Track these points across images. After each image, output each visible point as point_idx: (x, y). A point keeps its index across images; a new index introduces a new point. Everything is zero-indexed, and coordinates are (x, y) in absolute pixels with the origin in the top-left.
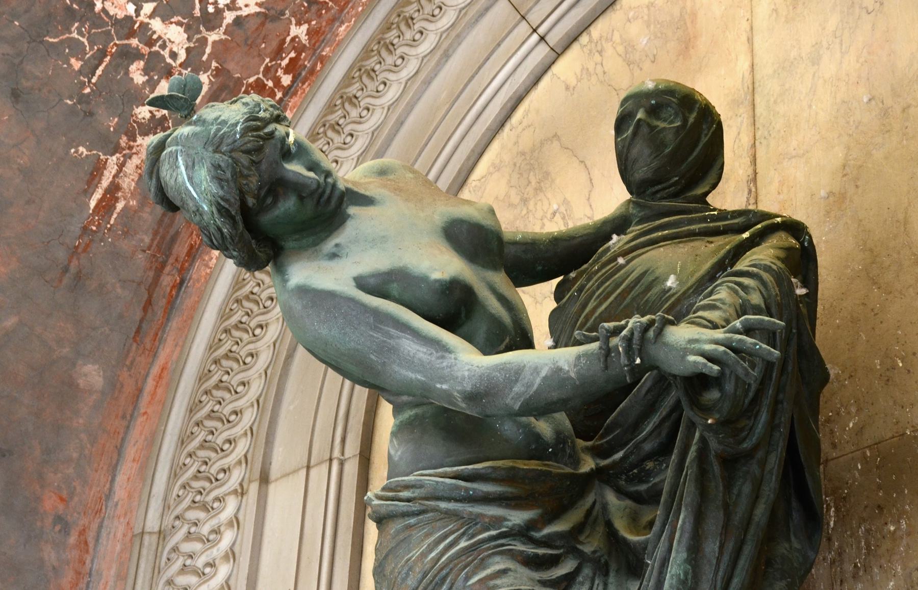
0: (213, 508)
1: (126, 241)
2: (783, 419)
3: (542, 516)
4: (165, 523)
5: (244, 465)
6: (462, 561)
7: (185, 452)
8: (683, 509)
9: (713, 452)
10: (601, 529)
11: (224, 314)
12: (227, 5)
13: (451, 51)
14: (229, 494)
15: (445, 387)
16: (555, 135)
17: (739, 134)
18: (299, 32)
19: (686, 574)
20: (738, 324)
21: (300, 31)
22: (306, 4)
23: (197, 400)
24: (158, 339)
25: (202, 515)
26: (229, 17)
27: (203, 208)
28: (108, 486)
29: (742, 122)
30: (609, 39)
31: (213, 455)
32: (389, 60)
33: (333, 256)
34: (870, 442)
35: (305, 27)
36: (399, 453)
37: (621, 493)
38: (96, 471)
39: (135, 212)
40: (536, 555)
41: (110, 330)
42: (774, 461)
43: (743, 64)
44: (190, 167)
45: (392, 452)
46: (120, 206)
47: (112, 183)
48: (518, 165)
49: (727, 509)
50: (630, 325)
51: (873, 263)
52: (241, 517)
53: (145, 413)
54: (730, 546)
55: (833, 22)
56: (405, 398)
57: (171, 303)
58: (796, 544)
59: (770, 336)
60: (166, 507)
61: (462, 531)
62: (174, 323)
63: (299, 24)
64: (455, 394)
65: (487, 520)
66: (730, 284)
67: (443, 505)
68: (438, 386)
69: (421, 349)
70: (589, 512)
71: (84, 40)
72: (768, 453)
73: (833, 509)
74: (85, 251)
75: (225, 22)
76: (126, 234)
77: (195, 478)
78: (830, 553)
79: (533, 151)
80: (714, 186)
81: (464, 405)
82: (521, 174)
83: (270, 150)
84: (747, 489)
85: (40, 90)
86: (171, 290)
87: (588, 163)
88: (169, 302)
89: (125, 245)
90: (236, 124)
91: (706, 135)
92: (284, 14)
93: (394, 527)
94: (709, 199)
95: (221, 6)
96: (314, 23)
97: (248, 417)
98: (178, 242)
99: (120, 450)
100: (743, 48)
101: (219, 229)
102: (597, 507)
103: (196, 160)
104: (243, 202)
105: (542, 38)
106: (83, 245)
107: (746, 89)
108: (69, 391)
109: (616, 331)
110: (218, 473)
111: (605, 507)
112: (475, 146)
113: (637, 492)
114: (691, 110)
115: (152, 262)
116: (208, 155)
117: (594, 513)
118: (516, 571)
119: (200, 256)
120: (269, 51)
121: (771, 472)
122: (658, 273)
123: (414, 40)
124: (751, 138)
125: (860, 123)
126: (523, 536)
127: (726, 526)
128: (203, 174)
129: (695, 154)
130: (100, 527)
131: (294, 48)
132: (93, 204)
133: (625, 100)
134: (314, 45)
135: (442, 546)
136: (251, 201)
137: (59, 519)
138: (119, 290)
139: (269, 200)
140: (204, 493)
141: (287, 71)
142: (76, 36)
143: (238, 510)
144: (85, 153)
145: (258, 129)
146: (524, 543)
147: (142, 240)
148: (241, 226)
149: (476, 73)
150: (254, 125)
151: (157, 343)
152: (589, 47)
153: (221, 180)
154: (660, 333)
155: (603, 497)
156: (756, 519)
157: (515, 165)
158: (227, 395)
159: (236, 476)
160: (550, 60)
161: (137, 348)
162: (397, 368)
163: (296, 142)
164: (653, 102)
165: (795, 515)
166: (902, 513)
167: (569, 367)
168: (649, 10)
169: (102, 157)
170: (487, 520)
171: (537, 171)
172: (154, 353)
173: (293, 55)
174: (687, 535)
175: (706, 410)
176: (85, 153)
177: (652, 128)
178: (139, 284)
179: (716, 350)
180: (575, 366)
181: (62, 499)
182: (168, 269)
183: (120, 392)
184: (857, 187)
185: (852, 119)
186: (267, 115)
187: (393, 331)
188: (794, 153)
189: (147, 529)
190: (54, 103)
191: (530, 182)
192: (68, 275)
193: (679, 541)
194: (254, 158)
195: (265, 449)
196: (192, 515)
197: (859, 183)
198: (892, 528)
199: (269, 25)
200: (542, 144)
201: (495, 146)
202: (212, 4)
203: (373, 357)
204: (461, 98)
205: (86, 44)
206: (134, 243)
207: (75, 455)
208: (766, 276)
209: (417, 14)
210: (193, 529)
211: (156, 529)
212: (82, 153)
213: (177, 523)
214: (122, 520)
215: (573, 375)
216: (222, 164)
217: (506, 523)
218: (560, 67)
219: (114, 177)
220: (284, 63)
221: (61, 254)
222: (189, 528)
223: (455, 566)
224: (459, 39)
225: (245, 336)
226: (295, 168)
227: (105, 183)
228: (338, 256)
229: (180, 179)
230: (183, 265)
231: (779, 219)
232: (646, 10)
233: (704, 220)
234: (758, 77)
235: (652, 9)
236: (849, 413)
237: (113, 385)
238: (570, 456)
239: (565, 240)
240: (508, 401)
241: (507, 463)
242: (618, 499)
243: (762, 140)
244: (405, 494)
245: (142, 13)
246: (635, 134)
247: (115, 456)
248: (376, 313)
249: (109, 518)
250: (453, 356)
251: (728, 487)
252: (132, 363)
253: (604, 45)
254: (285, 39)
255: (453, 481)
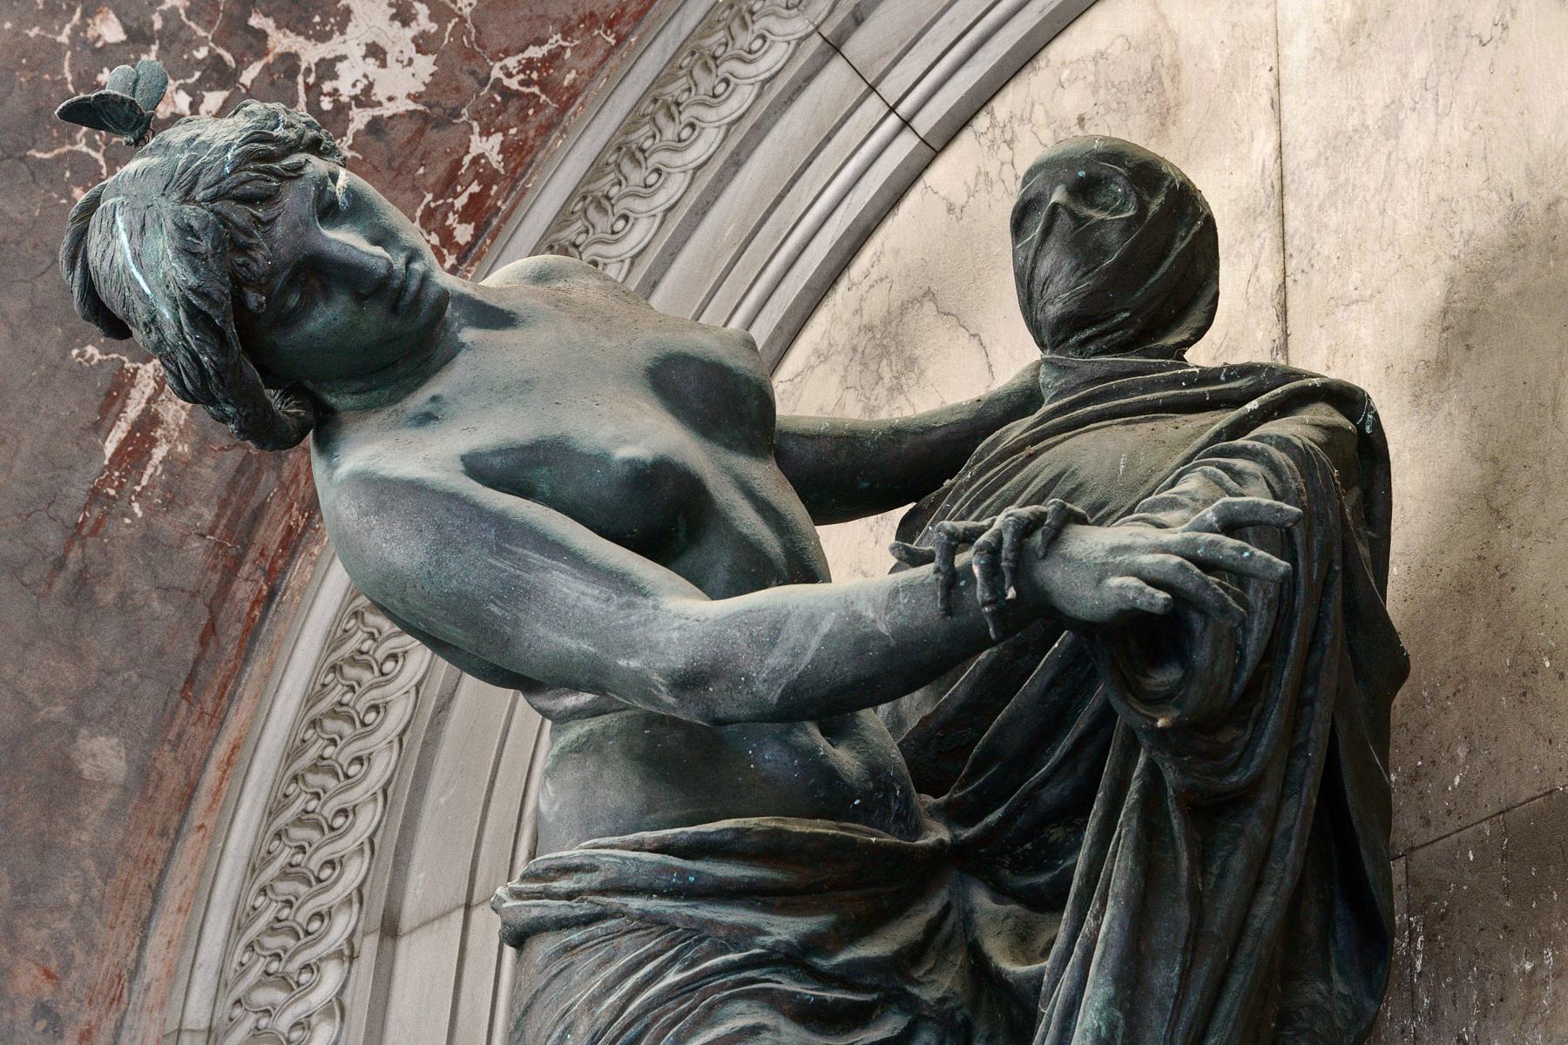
0: (298, 984)
1: (169, 517)
2: (1312, 734)
3: (836, 927)
4: (218, 1015)
5: (356, 907)
6: (669, 1011)
7: (256, 886)
8: (1110, 903)
9: (1171, 792)
10: (958, 959)
11: (334, 640)
12: (355, 98)
13: (742, 156)
14: (328, 957)
15: (634, 664)
16: (928, 292)
17: (1256, 267)
18: (487, 147)
19: (1112, 1027)
20: (1209, 514)
21: (488, 146)
22: (499, 99)
23: (280, 795)
24: (227, 692)
25: (280, 996)
26: (359, 119)
27: (162, 316)
28: (133, 954)
29: (1262, 247)
30: (1026, 119)
31: (303, 889)
32: (636, 176)
33: (426, 419)
34: (1491, 810)
35: (497, 139)
36: (556, 808)
37: (1001, 892)
38: (112, 928)
39: (187, 464)
40: (821, 1002)
41: (140, 676)
42: (1296, 814)
43: (1264, 146)
44: (140, 231)
45: (544, 807)
46: (159, 453)
47: (146, 411)
48: (860, 350)
49: (1199, 904)
50: (996, 525)
51: (1498, 482)
52: (347, 1000)
53: (202, 826)
54: (1203, 972)
55: (1420, 65)
56: (571, 701)
57: (252, 633)
58: (1341, 988)
59: (1279, 536)
60: (222, 985)
61: (672, 952)
62: (256, 668)
63: (486, 132)
64: (655, 677)
65: (722, 933)
66: (1208, 468)
67: (635, 904)
68: (622, 663)
69: (589, 591)
70: (934, 927)
71: (99, 156)
72: (1282, 798)
73: (1421, 938)
74: (94, 532)
75: (353, 128)
76: (169, 504)
77: (272, 930)
78: (1414, 1018)
79: (887, 322)
80: (1199, 334)
81: (671, 700)
82: (865, 365)
83: (295, 201)
84: (1238, 862)
85: (18, 243)
86: (252, 609)
87: (986, 341)
88: (246, 630)
89: (168, 525)
90: (227, 148)
91: (1183, 238)
92: (459, 116)
93: (543, 947)
94: (1189, 355)
95: (344, 99)
96: (513, 131)
97: (367, 819)
98: (266, 521)
99: (156, 892)
100: (1264, 117)
101: (195, 358)
102: (952, 918)
103: (149, 220)
104: (239, 302)
105: (906, 123)
106: (91, 522)
107: (1269, 188)
108: (63, 784)
109: (968, 538)
110: (310, 921)
111: (968, 919)
112: (784, 318)
113: (1033, 889)
114: (1153, 192)
115: (216, 557)
116: (167, 207)
117: (947, 928)
118: (777, 1031)
119: (305, 547)
120: (431, 180)
121: (1287, 835)
122: (1081, 475)
123: (680, 141)
124: (1279, 274)
125: (1471, 234)
126: (796, 965)
127: (1195, 938)
128: (162, 245)
129: (1162, 271)
130: (119, 1027)
131: (477, 176)
132: (110, 448)
133: (1031, 173)
134: (514, 171)
135: (629, 983)
136: (254, 299)
137: (43, 1010)
138: (155, 604)
139: (294, 300)
140: (285, 957)
141: (464, 217)
142: (85, 149)
143: (344, 987)
144: (98, 356)
145: (269, 157)
146: (798, 980)
147: (200, 516)
148: (237, 347)
149: (787, 189)
150: (265, 155)
151: (225, 702)
152: (990, 136)
153: (195, 255)
154: (1055, 538)
155: (966, 899)
156: (1256, 924)
157: (855, 350)
158: (331, 783)
159: (342, 925)
160: (915, 165)
161: (189, 711)
162: (541, 630)
163: (350, 191)
164: (1081, 174)
165: (1341, 933)
166: (1549, 939)
167: (875, 611)
168: (1096, 63)
169: (127, 365)
170: (722, 933)
171: (893, 358)
172: (218, 720)
173: (475, 188)
174: (1114, 952)
175: (1158, 701)
176: (98, 356)
177: (1078, 220)
178: (193, 595)
179: (1163, 562)
180: (888, 609)
181: (49, 975)
182: (246, 569)
183: (157, 788)
184: (1468, 347)
185: (1457, 229)
186: (292, 135)
187: (535, 557)
188: (1355, 295)
189: (188, 1025)
190: (43, 267)
191: (881, 378)
192: (63, 574)
193: (1100, 964)
194: (260, 213)
195: (393, 876)
196: (263, 997)
197: (1471, 342)
198: (1528, 967)
199: (432, 135)
200: (903, 309)
201: (821, 319)
202: (329, 94)
203: (495, 610)
204: (759, 235)
205: (102, 162)
206: (184, 520)
207: (74, 898)
208: (1280, 456)
209: (686, 95)
210: (264, 1022)
211: (204, 1025)
212: (92, 357)
213: (238, 1012)
214: (156, 1014)
215: (883, 628)
216: (195, 224)
217: (760, 939)
218: (938, 174)
219: (149, 401)
220: (460, 202)
221: (52, 538)
222: (258, 1020)
223: (656, 1019)
224: (760, 131)
225: (367, 677)
226: (346, 239)
227: (133, 411)
228: (436, 418)
229: (119, 260)
230: (273, 562)
231: (1316, 381)
232: (1091, 66)
233: (1174, 382)
234: (1290, 166)
235: (1102, 62)
236: (1453, 759)
237: (144, 776)
238: (899, 817)
239: (915, 433)
240: (759, 687)
241: (769, 822)
242: (995, 901)
243: (1299, 276)
244: (564, 884)
245: (203, 109)
246: (1046, 232)
247: (148, 903)
248: (501, 521)
249: (134, 1011)
250: (650, 602)
251: (1201, 861)
252: (179, 736)
253: (1016, 128)
254: (461, 159)
255: (657, 857)
